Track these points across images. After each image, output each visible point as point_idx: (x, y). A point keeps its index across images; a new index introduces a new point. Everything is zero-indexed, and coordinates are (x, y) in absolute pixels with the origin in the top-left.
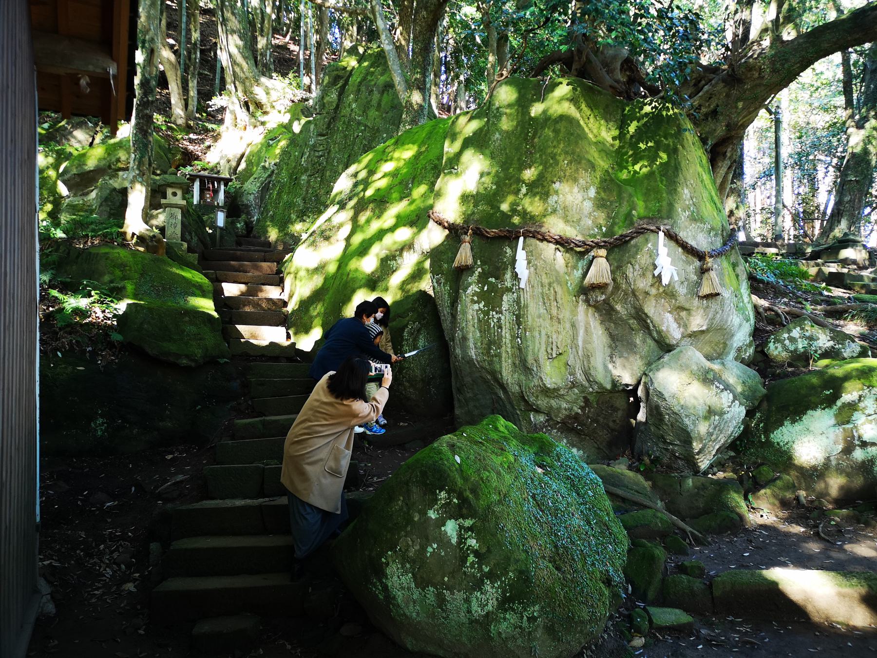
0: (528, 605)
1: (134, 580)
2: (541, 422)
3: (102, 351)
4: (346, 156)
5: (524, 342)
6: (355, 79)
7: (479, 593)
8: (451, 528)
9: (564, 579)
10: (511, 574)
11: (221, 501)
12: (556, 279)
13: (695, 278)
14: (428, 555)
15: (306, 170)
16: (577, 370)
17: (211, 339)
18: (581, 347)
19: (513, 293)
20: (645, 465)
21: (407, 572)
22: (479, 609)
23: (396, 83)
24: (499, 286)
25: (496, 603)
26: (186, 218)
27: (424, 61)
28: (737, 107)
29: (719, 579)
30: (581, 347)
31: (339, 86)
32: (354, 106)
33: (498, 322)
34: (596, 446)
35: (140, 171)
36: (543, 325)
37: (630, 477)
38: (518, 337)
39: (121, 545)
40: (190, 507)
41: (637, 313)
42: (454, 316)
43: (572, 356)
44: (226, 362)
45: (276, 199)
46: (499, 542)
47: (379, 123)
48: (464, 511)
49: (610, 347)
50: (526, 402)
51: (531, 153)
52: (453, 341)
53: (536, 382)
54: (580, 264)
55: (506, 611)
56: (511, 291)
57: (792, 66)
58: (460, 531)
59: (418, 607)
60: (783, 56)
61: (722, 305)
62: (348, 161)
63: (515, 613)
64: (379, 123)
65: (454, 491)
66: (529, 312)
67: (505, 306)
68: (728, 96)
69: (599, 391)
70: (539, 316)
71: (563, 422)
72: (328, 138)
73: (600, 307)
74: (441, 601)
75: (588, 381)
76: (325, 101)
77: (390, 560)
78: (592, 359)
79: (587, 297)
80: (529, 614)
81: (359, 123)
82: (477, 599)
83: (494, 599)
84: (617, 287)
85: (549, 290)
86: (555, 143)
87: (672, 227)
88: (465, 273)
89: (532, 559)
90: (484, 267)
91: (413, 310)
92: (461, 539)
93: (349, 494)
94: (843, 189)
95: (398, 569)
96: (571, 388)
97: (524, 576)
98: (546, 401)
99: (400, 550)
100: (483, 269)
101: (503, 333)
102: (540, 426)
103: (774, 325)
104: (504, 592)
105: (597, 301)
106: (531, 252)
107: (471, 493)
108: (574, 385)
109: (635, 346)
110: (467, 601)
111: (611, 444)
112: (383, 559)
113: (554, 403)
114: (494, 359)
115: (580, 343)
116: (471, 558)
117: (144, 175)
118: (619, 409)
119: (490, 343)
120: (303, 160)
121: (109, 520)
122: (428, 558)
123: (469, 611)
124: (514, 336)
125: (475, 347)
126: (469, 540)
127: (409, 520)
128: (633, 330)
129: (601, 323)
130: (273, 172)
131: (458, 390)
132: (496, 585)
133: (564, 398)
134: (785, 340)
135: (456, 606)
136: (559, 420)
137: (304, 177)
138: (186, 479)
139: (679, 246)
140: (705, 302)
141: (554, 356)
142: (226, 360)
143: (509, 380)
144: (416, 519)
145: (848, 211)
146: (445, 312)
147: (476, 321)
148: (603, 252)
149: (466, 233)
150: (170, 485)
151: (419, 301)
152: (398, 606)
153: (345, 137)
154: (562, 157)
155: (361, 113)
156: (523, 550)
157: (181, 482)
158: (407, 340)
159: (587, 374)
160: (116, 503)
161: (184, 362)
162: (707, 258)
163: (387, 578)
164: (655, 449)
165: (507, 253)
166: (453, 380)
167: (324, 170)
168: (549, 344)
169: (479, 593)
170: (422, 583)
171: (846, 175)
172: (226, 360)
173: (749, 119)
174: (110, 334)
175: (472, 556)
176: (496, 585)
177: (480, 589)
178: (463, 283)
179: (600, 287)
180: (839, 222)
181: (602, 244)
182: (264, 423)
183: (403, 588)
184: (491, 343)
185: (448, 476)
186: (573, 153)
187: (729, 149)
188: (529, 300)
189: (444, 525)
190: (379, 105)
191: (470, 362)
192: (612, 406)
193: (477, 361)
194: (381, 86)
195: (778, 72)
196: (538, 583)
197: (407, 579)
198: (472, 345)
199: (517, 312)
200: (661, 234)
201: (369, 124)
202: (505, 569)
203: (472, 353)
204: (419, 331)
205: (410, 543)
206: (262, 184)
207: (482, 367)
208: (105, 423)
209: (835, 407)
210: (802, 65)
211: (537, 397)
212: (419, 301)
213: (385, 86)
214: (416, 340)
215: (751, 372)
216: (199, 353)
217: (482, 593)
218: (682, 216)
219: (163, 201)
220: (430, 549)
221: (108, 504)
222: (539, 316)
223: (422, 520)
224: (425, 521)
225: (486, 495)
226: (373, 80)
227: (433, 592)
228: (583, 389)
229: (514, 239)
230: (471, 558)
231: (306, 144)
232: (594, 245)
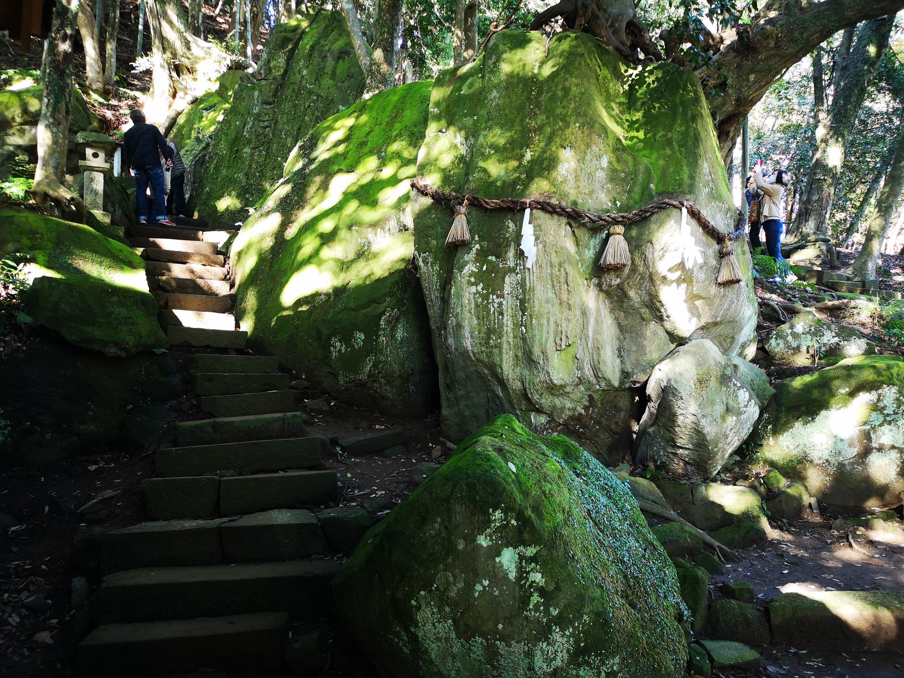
0: (607, 657)
1: (51, 628)
2: (542, 424)
3: (5, 336)
4: (296, 128)
5: (530, 331)
6: (306, 44)
7: (545, 644)
8: (508, 559)
9: (642, 619)
10: (585, 617)
11: (166, 523)
12: (568, 258)
13: (715, 262)
14: (477, 594)
15: (249, 142)
16: (585, 364)
17: (145, 325)
18: (591, 339)
19: (517, 274)
20: (651, 471)
21: (445, 619)
22: (545, 665)
23: (357, 46)
24: (501, 266)
25: (566, 656)
26: (108, 186)
27: (392, 20)
28: (748, 80)
29: (777, 604)
30: (591, 339)
31: (287, 49)
32: (305, 72)
33: (499, 307)
34: (596, 450)
35: (54, 118)
36: (551, 311)
37: (644, 486)
38: (522, 325)
39: (31, 581)
40: (126, 531)
41: (651, 301)
42: (445, 300)
43: (581, 348)
44: (163, 353)
45: (213, 174)
46: (569, 575)
47: (335, 94)
48: (526, 536)
49: (619, 339)
50: (529, 400)
51: (535, 114)
52: (445, 329)
53: (542, 377)
54: (592, 243)
55: (579, 666)
56: (515, 271)
57: (812, 36)
58: (521, 563)
59: (458, 664)
60: (803, 24)
61: (738, 295)
62: (298, 134)
63: (592, 669)
64: (335, 94)
65: (512, 509)
66: (536, 296)
67: (507, 289)
68: (739, 67)
69: (606, 388)
70: (547, 301)
71: (565, 424)
72: (274, 107)
73: (612, 293)
74: (492, 654)
75: (597, 377)
76: (271, 65)
77: (423, 602)
78: (602, 352)
79: (600, 281)
80: (608, 669)
81: (311, 92)
83: (565, 651)
84: (634, 269)
85: (559, 270)
86: (565, 103)
87: (694, 205)
88: (459, 249)
89: (608, 597)
90: (482, 243)
91: (390, 294)
92: (522, 573)
93: (329, 510)
94: (811, 187)
95: (433, 613)
96: (577, 385)
97: (602, 620)
98: (549, 400)
99: (437, 588)
100: (481, 246)
101: (505, 320)
102: (541, 428)
103: (771, 321)
104: (577, 642)
105: (610, 286)
106: (540, 226)
107: (533, 512)
108: (581, 381)
110: (529, 654)
111: (611, 449)
112: (413, 602)
113: (558, 402)
114: (494, 350)
115: (591, 334)
116: (535, 598)
117: (59, 124)
118: (622, 410)
119: (490, 332)
120: (246, 129)
121: (15, 549)
122: (475, 599)
123: (531, 668)
124: (517, 324)
125: (471, 336)
126: (532, 574)
127: (450, 549)
128: (644, 320)
129: (610, 312)
130: (208, 145)
131: (448, 386)
132: (567, 633)
133: (569, 397)
134: (787, 336)
135: (512, 662)
136: (561, 421)
137: (247, 150)
138: (116, 495)
139: (700, 225)
140: (722, 290)
141: (563, 347)
142: (163, 350)
143: (510, 375)
144: (461, 547)
145: (816, 210)
146: (433, 297)
147: (473, 306)
148: (620, 229)
149: (461, 204)
150: (96, 503)
151: (398, 285)
152: (432, 662)
153: (295, 106)
154: (573, 119)
156: (596, 585)
157: (111, 498)
158: (384, 329)
159: (596, 369)
160: (24, 527)
161: (112, 350)
162: (727, 240)
163: (417, 626)
164: (662, 453)
165: (509, 228)
166: (440, 375)
167: (270, 142)
168: (558, 333)
169: (545, 644)
170: (465, 631)
171: (815, 174)
172: (163, 350)
173: (759, 95)
174: (16, 314)
175: (536, 595)
176: (567, 633)
177: (547, 639)
178: (458, 261)
179: (617, 269)
180: (807, 221)
181: (620, 219)
182: (214, 425)
183: (439, 639)
184: (491, 332)
185: (504, 489)
186: (585, 115)
187: (733, 129)
188: (535, 282)
189: (499, 555)
190: (334, 72)
191: (465, 354)
192: (616, 406)
193: (473, 353)
194: (336, 52)
195: (796, 41)
196: (617, 627)
197: (445, 628)
198: (467, 335)
199: (521, 297)
200: (684, 210)
202: (579, 611)
203: (468, 343)
204: (397, 319)
205: (451, 579)
206: (195, 157)
207: (478, 360)
208: (8, 426)
210: (822, 34)
211: (542, 394)
212: (398, 285)
213: (341, 53)
214: (393, 329)
215: (756, 367)
216: (131, 340)
217: (548, 644)
218: (703, 192)
219: (81, 163)
220: (479, 588)
221: (13, 529)
222: (547, 301)
223: (469, 549)
224: (473, 550)
225: (551, 515)
226: (326, 45)
227: (481, 643)
228: (589, 386)
229: (518, 211)
230: (535, 598)
231: (249, 113)
232: (610, 220)
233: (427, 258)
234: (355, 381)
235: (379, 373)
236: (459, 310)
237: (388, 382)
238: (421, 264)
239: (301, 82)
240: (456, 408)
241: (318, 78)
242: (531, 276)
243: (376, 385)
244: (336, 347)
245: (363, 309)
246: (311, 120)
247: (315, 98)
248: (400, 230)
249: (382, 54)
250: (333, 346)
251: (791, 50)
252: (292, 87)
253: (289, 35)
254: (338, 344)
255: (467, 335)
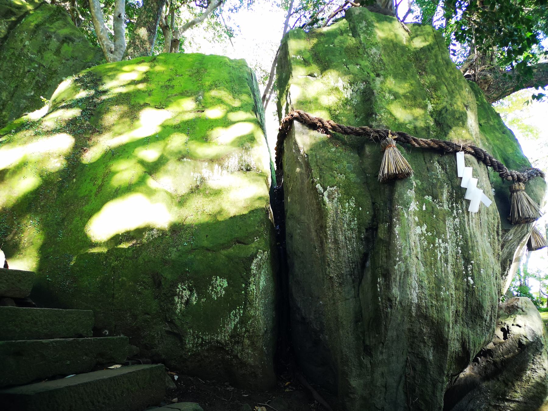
4: (13, 85)
5: (479, 282)
19: (454, 218)
31: (10, 20)
33: (445, 253)
81: (32, 60)
147: (419, 250)
155: (36, 52)
188: (475, 228)
194: (61, 36)
199: (461, 243)
201: (44, 64)
233: (333, 193)
234: (210, 342)
235: (247, 331)
236: (407, 253)
237: (253, 343)
238: (326, 199)
239: (22, 49)
240: (369, 377)
241: (41, 50)
242: (470, 222)
243: (238, 348)
244: (182, 298)
245: (223, 249)
246: (30, 82)
247: (36, 65)
248: (239, 170)
249: (146, 32)
250: (178, 295)
251: (495, 95)
252: (12, 51)
253: (14, 10)
254: (186, 293)
255: (414, 284)
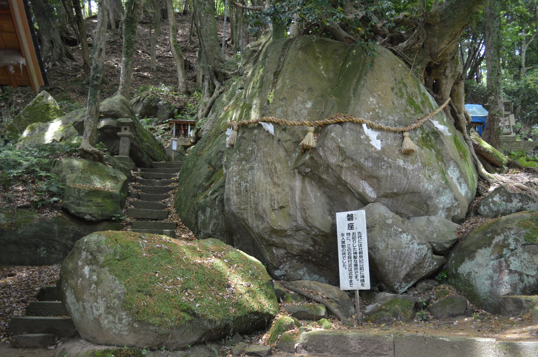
2: (282, 254)
82: (95, 306)
92: (91, 276)
102: (281, 256)
109: (347, 204)
115: (297, 200)
116: (93, 286)
132: (103, 299)
141: (276, 208)
161: (87, 217)
189: (84, 268)
209: (492, 246)
220: (79, 282)
